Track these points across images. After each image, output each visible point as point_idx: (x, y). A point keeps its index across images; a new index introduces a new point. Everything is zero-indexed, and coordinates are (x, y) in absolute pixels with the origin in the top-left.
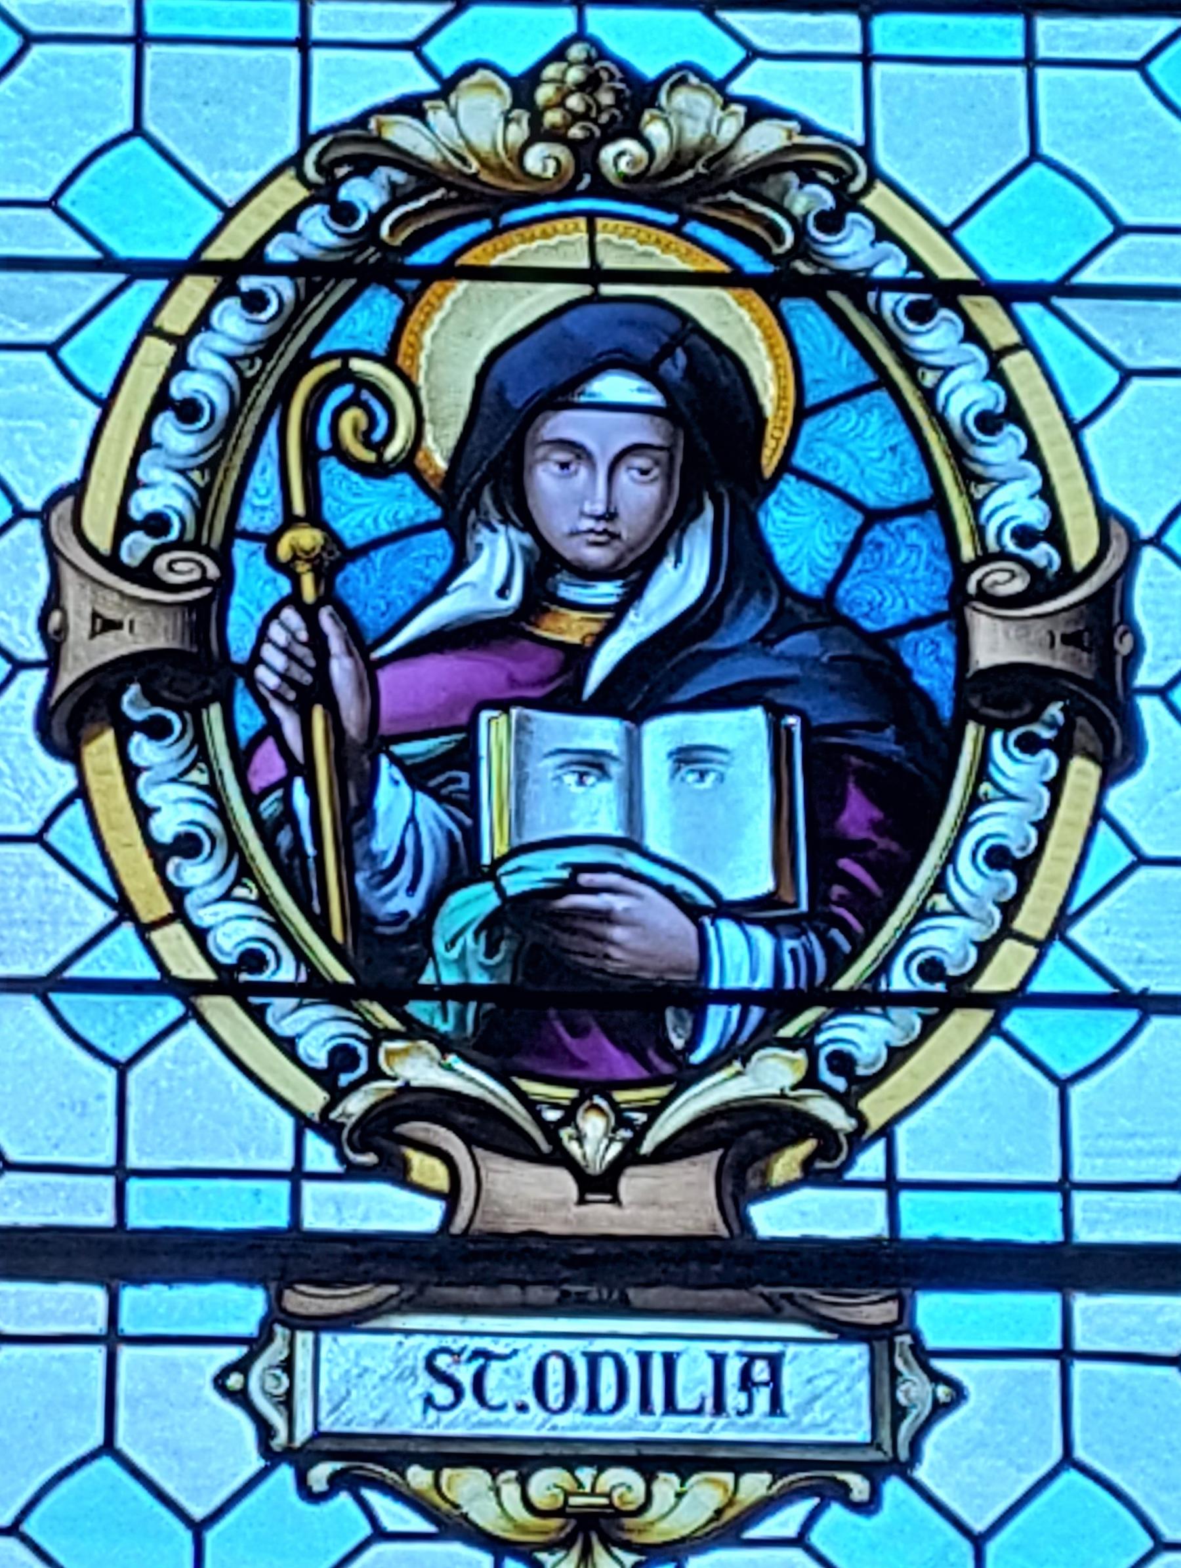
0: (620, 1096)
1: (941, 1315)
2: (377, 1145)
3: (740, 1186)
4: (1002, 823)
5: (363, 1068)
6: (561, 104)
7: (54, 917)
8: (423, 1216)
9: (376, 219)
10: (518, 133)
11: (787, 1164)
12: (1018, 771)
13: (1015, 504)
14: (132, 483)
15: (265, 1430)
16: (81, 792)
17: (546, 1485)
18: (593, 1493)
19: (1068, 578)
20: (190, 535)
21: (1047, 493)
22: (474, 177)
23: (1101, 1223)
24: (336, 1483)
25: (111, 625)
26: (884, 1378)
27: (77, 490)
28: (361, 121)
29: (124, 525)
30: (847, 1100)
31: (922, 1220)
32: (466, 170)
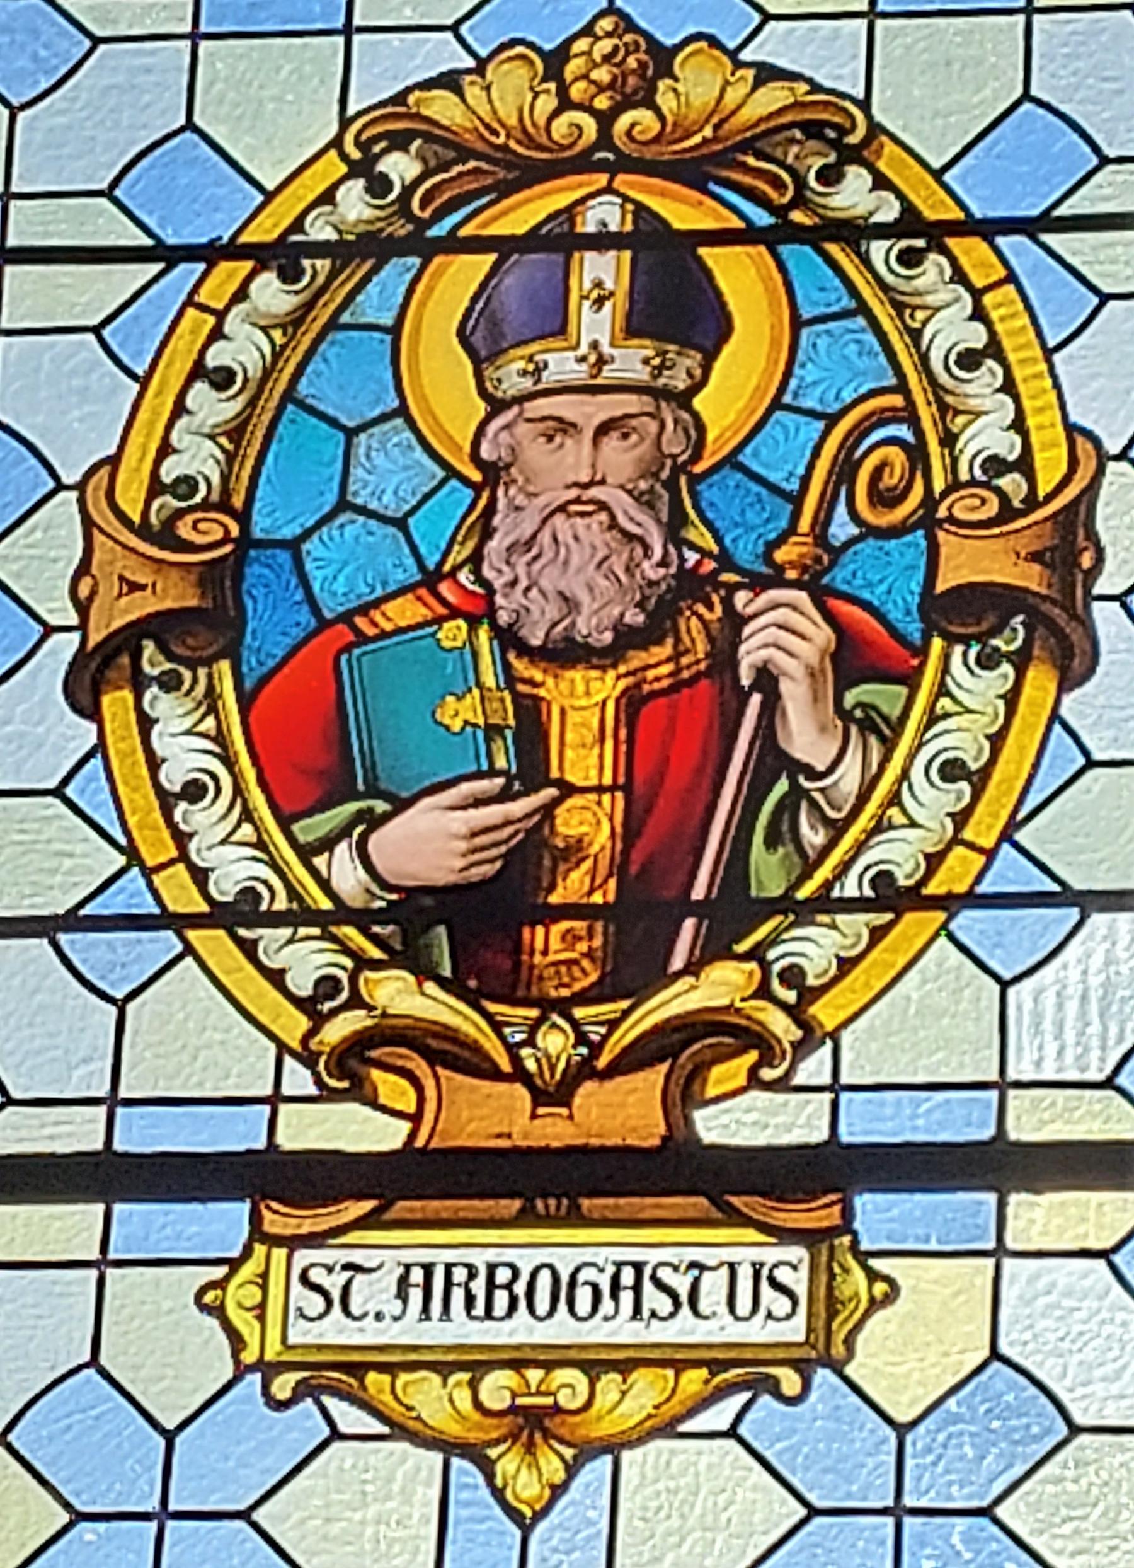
0: (579, 1013)
1: (878, 1214)
2: (346, 1074)
3: (684, 1095)
4: (963, 739)
5: (345, 995)
6: (585, 77)
7: (68, 865)
8: (390, 1135)
9: (408, 190)
10: (547, 103)
11: (729, 1073)
12: (980, 689)
13: (987, 436)
14: (165, 449)
15: (237, 1341)
16: (100, 747)
17: (497, 1388)
18: (539, 1393)
19: (1032, 502)
20: (215, 497)
21: (1019, 425)
22: (505, 148)
23: (1033, 1122)
24: (300, 1392)
25: (134, 587)
26: (824, 1276)
27: (113, 461)
28: (400, 98)
29: (156, 487)
30: (794, 1012)
31: (866, 1124)
32: (493, 139)
